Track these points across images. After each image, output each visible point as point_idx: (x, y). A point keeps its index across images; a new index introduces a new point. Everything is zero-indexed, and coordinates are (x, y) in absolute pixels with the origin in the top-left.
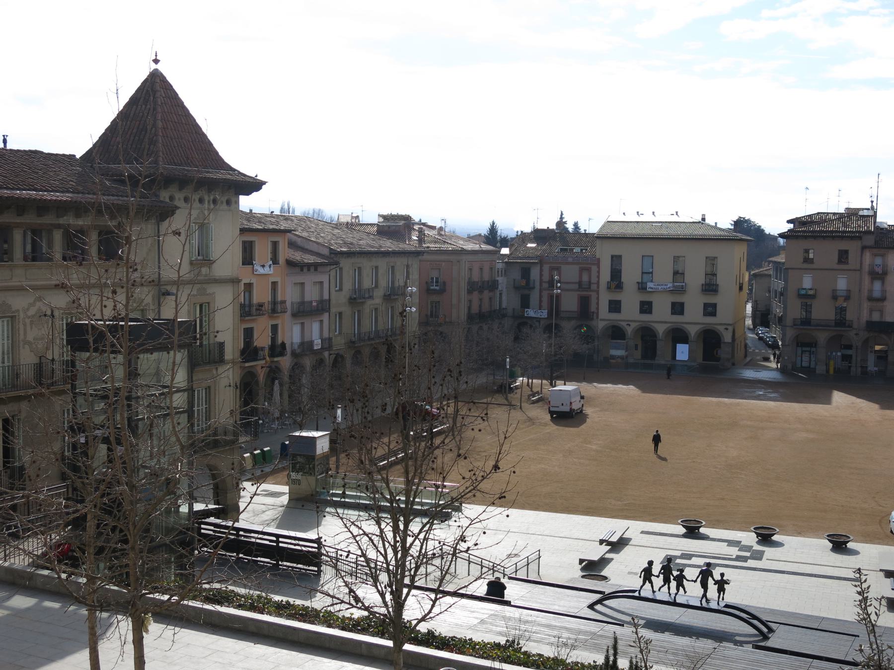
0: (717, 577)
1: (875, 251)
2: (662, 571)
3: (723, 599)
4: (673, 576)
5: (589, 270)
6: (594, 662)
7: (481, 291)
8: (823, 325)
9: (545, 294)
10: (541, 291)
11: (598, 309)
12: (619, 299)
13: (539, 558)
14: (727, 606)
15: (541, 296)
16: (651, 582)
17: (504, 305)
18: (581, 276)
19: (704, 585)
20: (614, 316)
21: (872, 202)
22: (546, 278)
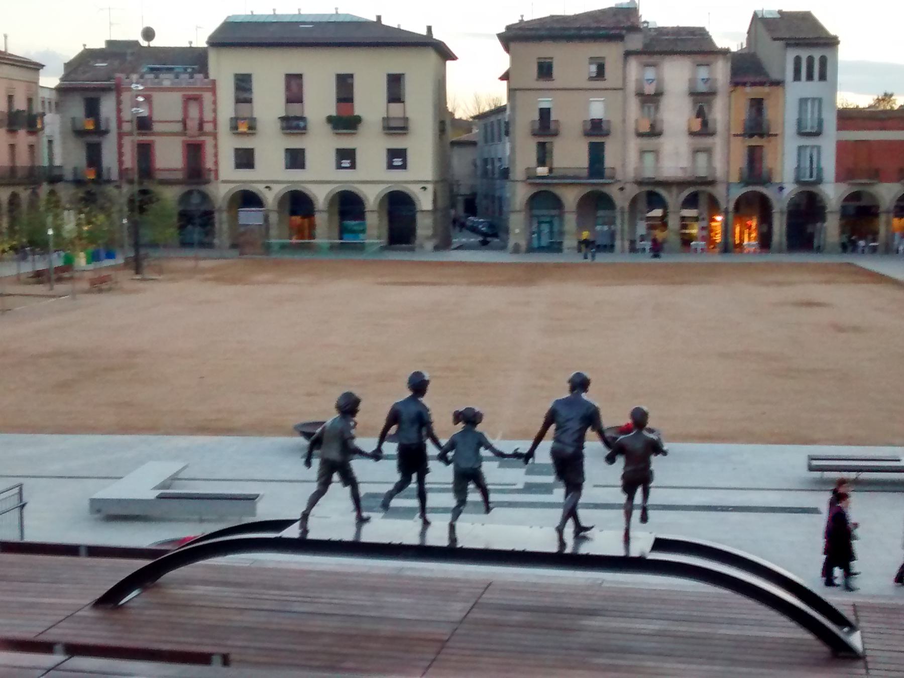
1: (645, 59)
2: (393, 430)
4: (436, 441)
5: (197, 99)
10: (121, 135)
11: (216, 163)
12: (252, 147)
13: (22, 507)
14: (660, 544)
15: (120, 146)
16: (349, 480)
17: (57, 162)
20: (244, 175)
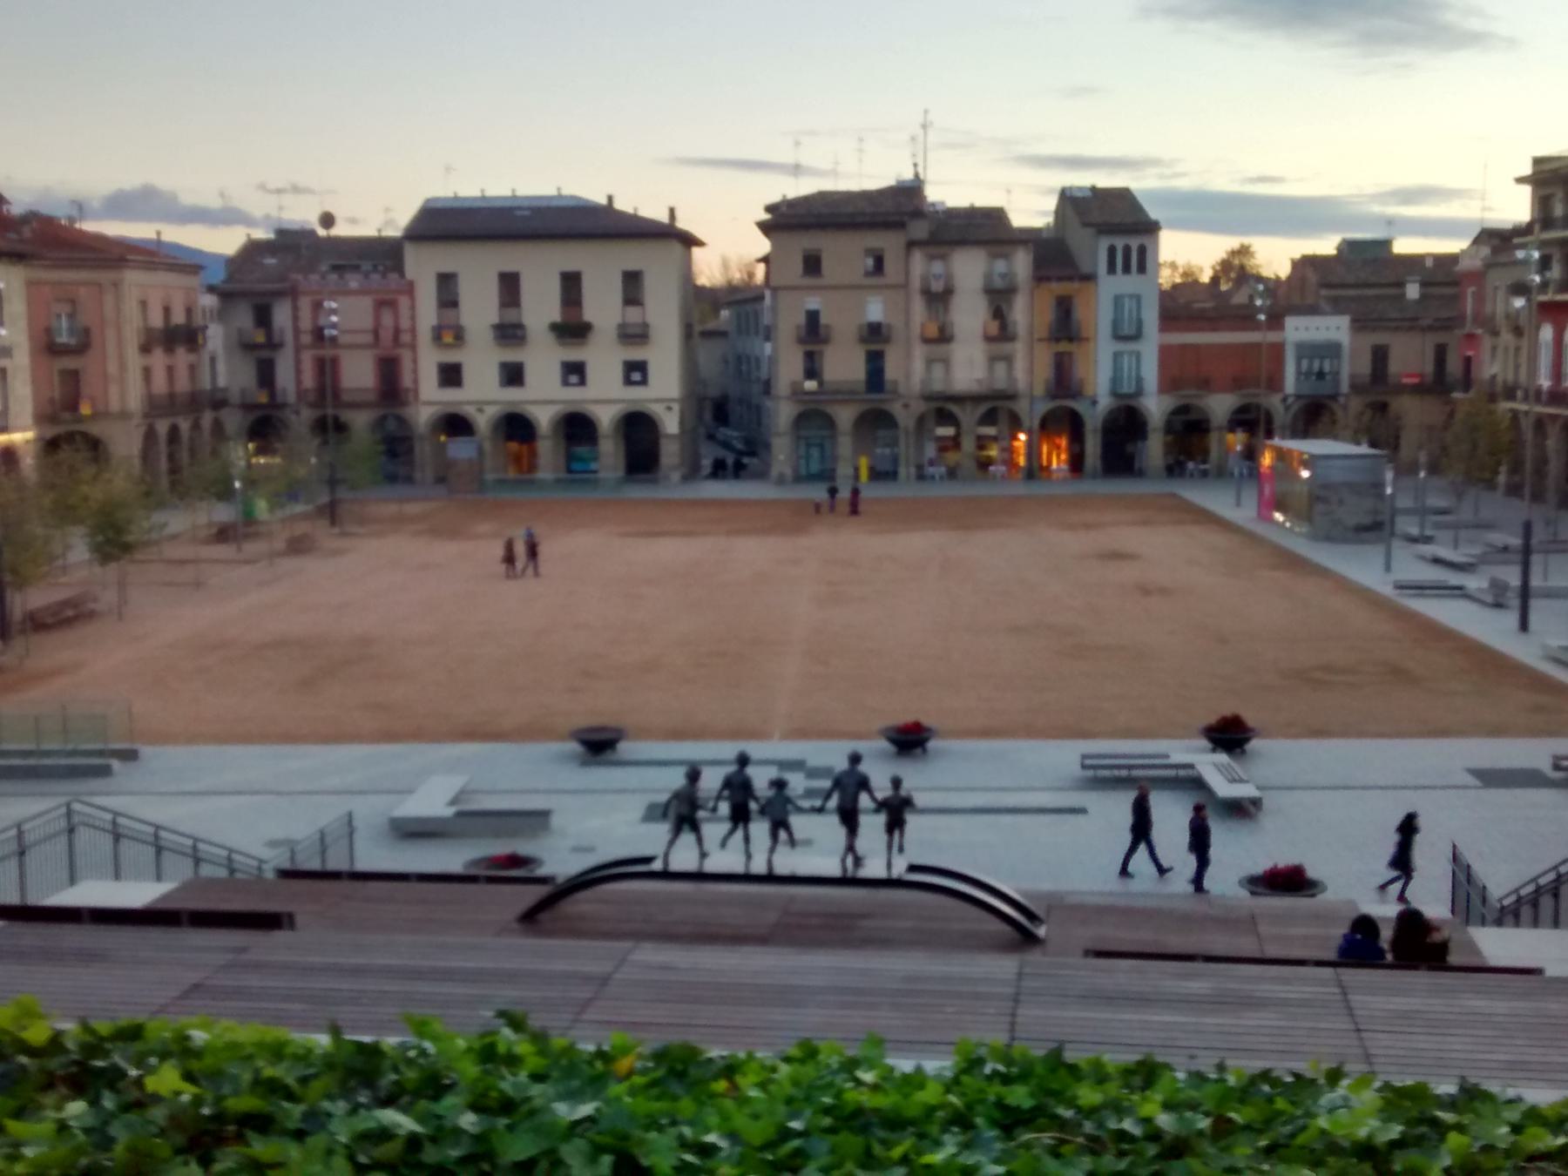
0: (883, 790)
3: (901, 849)
6: (328, 220)
7: (169, 348)
8: (843, 394)
9: (308, 359)
14: (913, 868)
15: (298, 362)
17: (222, 382)
18: (377, 318)
19: (849, 817)
20: (451, 395)
21: (915, 165)
22: (306, 323)
